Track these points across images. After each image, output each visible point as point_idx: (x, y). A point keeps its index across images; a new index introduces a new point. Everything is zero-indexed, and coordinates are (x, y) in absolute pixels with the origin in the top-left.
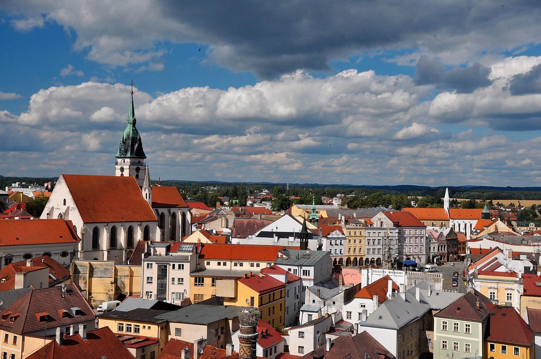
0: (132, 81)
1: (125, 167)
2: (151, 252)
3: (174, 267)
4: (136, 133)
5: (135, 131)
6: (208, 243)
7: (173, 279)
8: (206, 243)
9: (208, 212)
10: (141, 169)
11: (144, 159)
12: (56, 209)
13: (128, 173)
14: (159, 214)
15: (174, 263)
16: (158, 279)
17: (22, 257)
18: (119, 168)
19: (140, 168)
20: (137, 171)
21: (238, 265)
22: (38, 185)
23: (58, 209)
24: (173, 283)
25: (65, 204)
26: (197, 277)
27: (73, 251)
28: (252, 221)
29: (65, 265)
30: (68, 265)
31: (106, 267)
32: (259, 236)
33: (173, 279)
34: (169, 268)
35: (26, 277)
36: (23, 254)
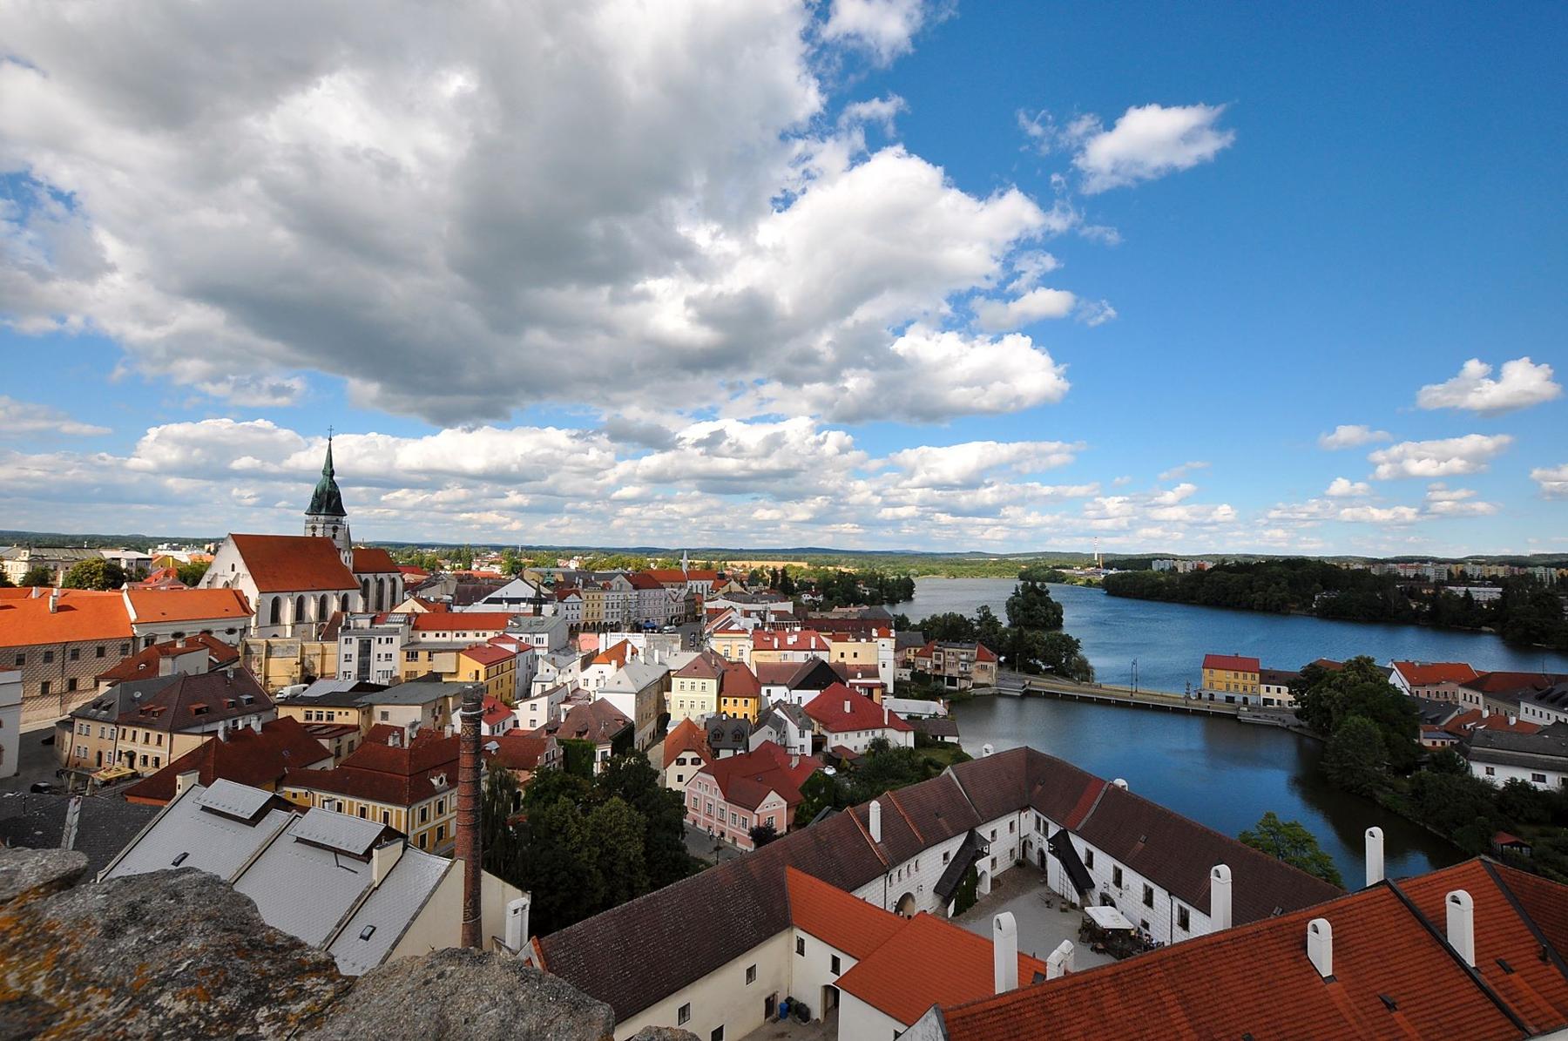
7: (379, 656)
25: (233, 570)
33: (379, 656)
34: (374, 643)
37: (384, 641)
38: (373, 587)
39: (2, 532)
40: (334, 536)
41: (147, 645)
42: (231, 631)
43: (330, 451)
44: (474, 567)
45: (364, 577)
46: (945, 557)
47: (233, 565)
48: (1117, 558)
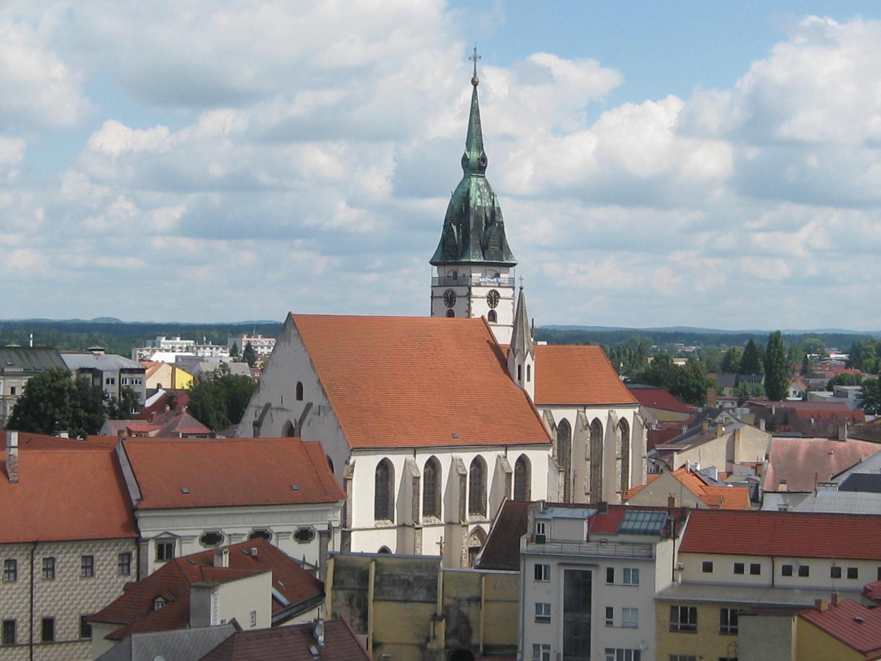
0: (475, 49)
1: (502, 292)
2: (543, 532)
3: (610, 579)
4: (488, 194)
5: (485, 191)
6: (699, 507)
7: (609, 612)
8: (695, 507)
9: (684, 417)
10: (501, 295)
11: (511, 268)
12: (277, 409)
13: (472, 305)
14: (554, 424)
15: (610, 566)
16: (565, 610)
17: (197, 540)
18: (442, 295)
19: (498, 294)
20: (492, 302)
21: (795, 573)
22: (211, 343)
23: (282, 409)
24: (609, 623)
25: (300, 396)
26: (676, 605)
27: (326, 528)
28: (820, 446)
29: (307, 564)
30: (314, 564)
31: (417, 574)
32: (844, 488)
33: (609, 612)
34: (598, 579)
35: (217, 597)
36: (199, 533)
37: (618, 576)
38: (581, 442)
39: (10, 329)
40: (493, 316)
41: (160, 557)
42: (304, 536)
43: (475, 111)
44: (793, 395)
45: (558, 415)
46: (75, 352)
47: (300, 387)
48: (268, 323)
